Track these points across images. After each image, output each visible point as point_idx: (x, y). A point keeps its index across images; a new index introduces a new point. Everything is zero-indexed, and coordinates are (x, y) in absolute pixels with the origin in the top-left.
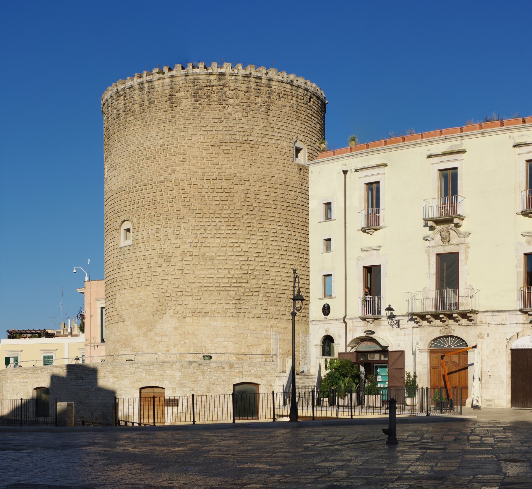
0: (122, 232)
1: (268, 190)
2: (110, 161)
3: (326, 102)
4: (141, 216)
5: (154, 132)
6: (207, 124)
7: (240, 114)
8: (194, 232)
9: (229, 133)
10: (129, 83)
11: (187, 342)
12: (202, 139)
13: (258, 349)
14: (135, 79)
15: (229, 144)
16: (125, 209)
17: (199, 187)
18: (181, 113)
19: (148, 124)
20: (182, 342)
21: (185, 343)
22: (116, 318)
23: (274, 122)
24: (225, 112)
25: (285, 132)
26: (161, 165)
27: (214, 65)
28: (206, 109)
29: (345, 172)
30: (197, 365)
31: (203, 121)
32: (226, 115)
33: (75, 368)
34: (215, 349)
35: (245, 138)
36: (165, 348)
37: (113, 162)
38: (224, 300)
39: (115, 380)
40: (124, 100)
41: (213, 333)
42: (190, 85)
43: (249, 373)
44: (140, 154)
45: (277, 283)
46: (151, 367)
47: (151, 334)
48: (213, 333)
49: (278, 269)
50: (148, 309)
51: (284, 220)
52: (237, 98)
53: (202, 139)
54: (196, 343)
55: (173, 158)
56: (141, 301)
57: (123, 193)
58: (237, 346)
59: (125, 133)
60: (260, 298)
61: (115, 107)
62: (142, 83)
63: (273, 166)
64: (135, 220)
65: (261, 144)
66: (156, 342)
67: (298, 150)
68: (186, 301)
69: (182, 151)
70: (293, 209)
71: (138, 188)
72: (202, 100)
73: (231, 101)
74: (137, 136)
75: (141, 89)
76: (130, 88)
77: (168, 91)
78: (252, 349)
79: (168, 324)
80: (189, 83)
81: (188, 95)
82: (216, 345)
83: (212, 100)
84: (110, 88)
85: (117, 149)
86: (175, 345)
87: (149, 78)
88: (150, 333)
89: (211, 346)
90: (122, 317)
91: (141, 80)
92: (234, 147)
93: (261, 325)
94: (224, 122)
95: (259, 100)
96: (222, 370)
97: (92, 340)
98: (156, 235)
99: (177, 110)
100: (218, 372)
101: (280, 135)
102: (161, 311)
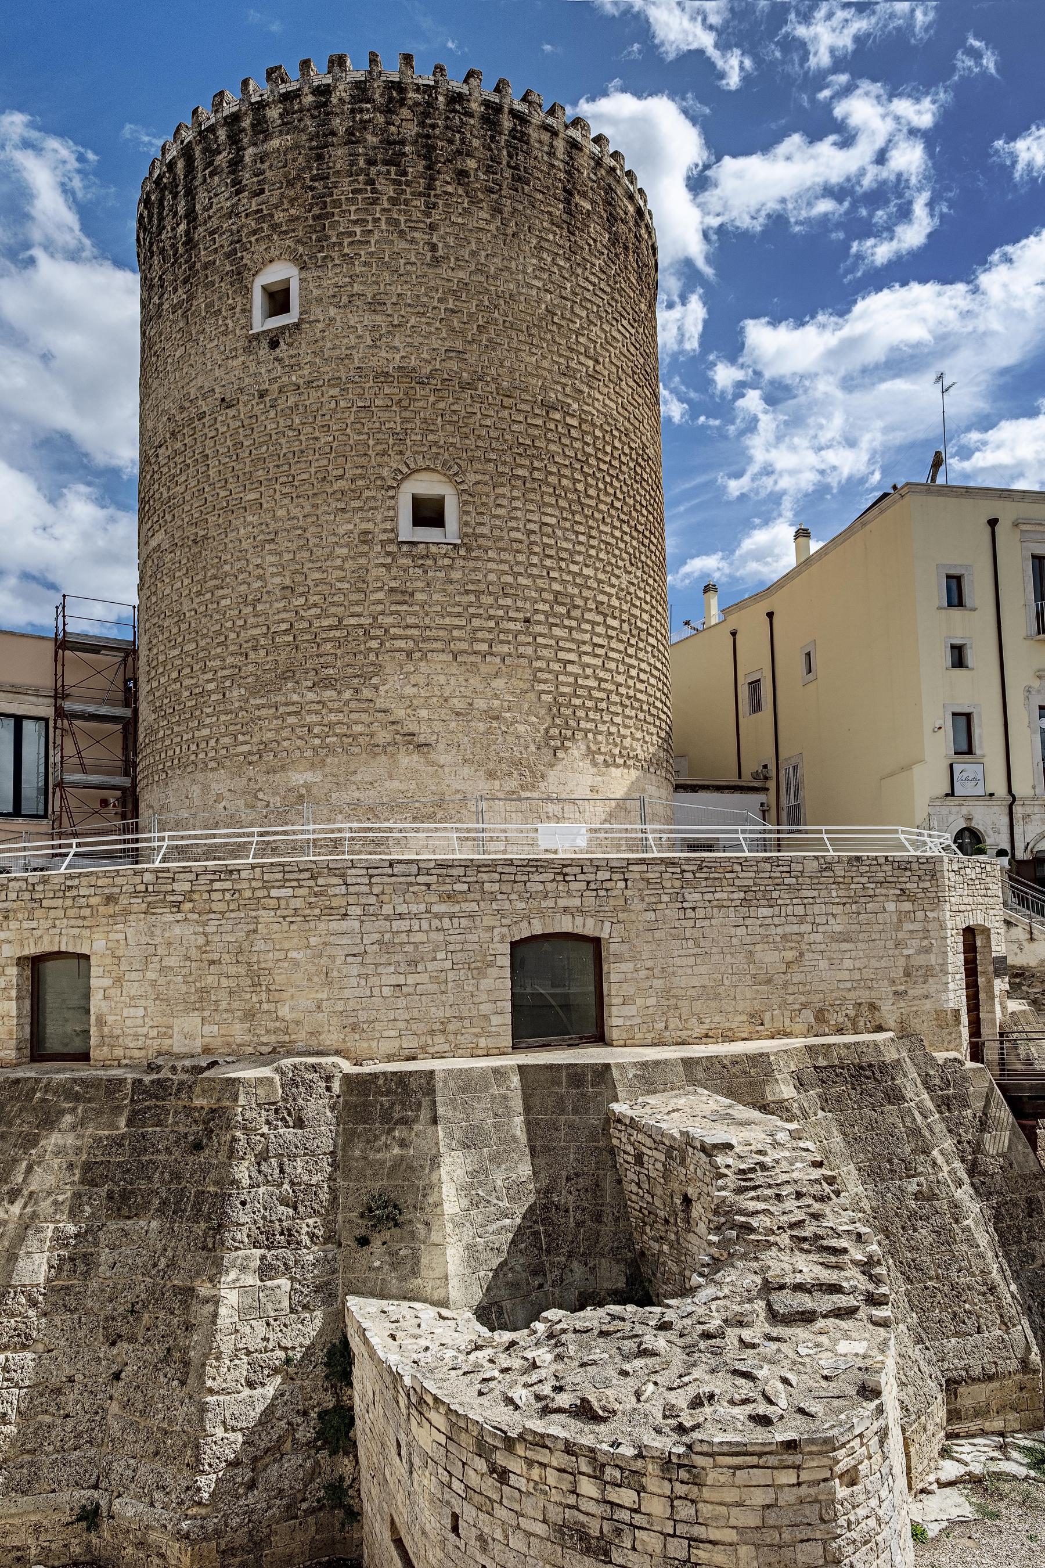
29: (993, 523)
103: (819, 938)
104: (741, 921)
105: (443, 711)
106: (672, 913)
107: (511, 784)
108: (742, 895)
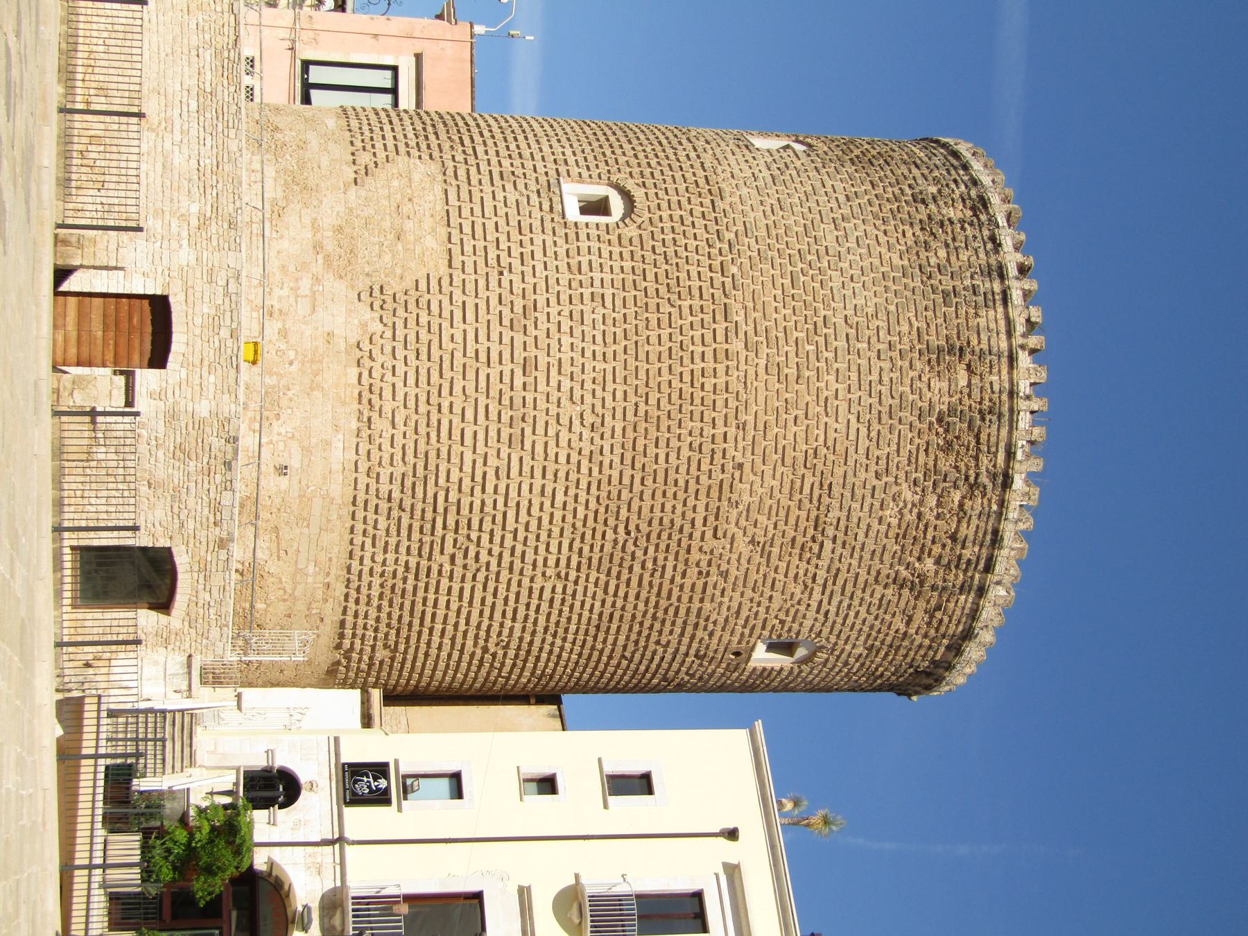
0: (598, 190)
1: (688, 582)
2: (798, 164)
3: (914, 698)
4: (640, 253)
5: (867, 299)
6: (875, 440)
7: (895, 522)
8: (588, 398)
9: (848, 494)
10: (1007, 239)
11: (294, 368)
12: (836, 425)
13: (267, 552)
14: (1019, 257)
15: (816, 492)
16: (664, 205)
17: (706, 413)
18: (912, 374)
19: (890, 284)
20: (292, 354)
21: (291, 363)
22: (365, 158)
23: (867, 598)
24: (905, 485)
25: (840, 620)
26: (775, 316)
27: (1036, 465)
28: (917, 441)
29: (732, 834)
30: (229, 457)
31: (885, 432)
32: (895, 489)
33: (232, 89)
34: (271, 442)
35: (830, 531)
36: (277, 306)
37: (794, 173)
38: (403, 469)
39: (194, 222)
40: (962, 221)
41: (314, 441)
42: (987, 403)
43: (201, 587)
44: (809, 258)
45: (443, 600)
46: (225, 333)
47: (318, 266)
48: (314, 441)
49: (477, 601)
50: (387, 258)
51: (606, 617)
52: (938, 517)
53: (836, 425)
54: (290, 394)
55: (791, 349)
56: (412, 238)
57: (707, 202)
58: (278, 501)
59: (870, 217)
60: (403, 558)
61: (946, 191)
62: (1002, 277)
63: (749, 593)
64: (631, 231)
65: (812, 569)
66: (297, 280)
67: (786, 648)
68: (404, 368)
69: (807, 373)
70: (633, 637)
71: (718, 245)
72: (941, 430)
73: (932, 500)
74: (860, 251)
75: (988, 272)
76: (993, 239)
77: (974, 342)
78: (267, 538)
79: (346, 319)
80: (991, 400)
81: (959, 395)
82: (281, 446)
83: (941, 454)
84: (1001, 178)
85: (830, 190)
86: (283, 333)
87: (1016, 296)
88: (320, 261)
89: (279, 434)
90: (369, 180)
91: (1012, 271)
92: (808, 506)
93: (330, 560)
94: (875, 482)
95: (929, 564)
96: (212, 519)
97: (311, 34)
98: (587, 292)
99: (918, 365)
100: (206, 510)
101: (833, 610)
102: (376, 296)
103: (168, 145)
104: (186, 87)
105: (399, 196)
106: (194, 41)
107: (330, 246)
108: (208, 90)
